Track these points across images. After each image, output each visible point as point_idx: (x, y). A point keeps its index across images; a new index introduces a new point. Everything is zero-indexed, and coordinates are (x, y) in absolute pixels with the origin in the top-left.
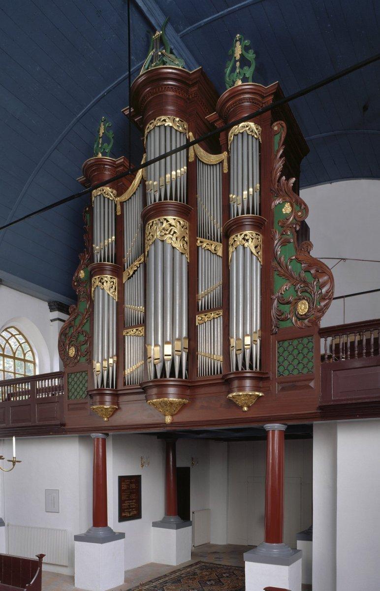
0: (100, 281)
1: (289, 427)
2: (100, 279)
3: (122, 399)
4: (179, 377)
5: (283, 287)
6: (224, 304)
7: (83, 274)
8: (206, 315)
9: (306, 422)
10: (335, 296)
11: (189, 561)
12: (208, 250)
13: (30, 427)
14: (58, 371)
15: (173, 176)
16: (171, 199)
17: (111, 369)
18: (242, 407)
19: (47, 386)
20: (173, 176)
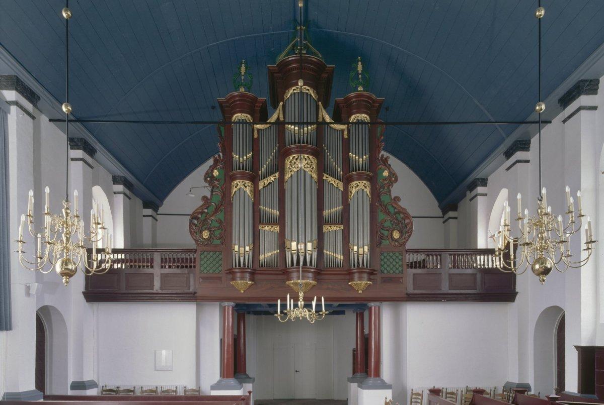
0: (244, 185)
1: (237, 305)
2: (244, 183)
3: (257, 277)
4: (297, 265)
5: (381, 216)
6: (344, 218)
7: (218, 174)
8: (330, 227)
9: (365, 303)
10: (190, 216)
11: (574, 393)
12: (332, 184)
13: (418, 294)
14: (123, 248)
15: (306, 132)
16: (307, 143)
17: (365, 256)
18: (358, 291)
19: (490, 266)
20: (306, 132)
